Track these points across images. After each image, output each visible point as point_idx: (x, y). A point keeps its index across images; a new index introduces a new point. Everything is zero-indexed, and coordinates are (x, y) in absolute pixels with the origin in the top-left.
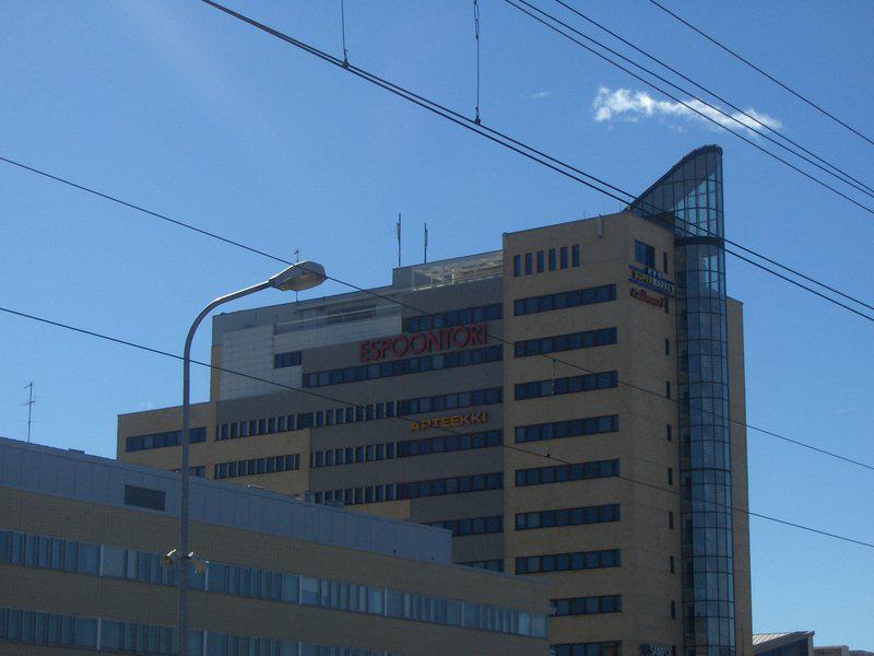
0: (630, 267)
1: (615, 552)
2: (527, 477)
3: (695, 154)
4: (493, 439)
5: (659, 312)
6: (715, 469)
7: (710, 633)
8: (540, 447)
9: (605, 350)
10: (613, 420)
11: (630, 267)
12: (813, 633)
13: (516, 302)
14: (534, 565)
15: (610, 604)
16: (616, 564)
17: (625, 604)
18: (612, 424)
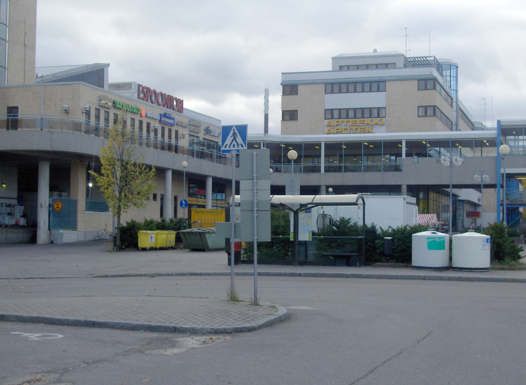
12: (108, 65)
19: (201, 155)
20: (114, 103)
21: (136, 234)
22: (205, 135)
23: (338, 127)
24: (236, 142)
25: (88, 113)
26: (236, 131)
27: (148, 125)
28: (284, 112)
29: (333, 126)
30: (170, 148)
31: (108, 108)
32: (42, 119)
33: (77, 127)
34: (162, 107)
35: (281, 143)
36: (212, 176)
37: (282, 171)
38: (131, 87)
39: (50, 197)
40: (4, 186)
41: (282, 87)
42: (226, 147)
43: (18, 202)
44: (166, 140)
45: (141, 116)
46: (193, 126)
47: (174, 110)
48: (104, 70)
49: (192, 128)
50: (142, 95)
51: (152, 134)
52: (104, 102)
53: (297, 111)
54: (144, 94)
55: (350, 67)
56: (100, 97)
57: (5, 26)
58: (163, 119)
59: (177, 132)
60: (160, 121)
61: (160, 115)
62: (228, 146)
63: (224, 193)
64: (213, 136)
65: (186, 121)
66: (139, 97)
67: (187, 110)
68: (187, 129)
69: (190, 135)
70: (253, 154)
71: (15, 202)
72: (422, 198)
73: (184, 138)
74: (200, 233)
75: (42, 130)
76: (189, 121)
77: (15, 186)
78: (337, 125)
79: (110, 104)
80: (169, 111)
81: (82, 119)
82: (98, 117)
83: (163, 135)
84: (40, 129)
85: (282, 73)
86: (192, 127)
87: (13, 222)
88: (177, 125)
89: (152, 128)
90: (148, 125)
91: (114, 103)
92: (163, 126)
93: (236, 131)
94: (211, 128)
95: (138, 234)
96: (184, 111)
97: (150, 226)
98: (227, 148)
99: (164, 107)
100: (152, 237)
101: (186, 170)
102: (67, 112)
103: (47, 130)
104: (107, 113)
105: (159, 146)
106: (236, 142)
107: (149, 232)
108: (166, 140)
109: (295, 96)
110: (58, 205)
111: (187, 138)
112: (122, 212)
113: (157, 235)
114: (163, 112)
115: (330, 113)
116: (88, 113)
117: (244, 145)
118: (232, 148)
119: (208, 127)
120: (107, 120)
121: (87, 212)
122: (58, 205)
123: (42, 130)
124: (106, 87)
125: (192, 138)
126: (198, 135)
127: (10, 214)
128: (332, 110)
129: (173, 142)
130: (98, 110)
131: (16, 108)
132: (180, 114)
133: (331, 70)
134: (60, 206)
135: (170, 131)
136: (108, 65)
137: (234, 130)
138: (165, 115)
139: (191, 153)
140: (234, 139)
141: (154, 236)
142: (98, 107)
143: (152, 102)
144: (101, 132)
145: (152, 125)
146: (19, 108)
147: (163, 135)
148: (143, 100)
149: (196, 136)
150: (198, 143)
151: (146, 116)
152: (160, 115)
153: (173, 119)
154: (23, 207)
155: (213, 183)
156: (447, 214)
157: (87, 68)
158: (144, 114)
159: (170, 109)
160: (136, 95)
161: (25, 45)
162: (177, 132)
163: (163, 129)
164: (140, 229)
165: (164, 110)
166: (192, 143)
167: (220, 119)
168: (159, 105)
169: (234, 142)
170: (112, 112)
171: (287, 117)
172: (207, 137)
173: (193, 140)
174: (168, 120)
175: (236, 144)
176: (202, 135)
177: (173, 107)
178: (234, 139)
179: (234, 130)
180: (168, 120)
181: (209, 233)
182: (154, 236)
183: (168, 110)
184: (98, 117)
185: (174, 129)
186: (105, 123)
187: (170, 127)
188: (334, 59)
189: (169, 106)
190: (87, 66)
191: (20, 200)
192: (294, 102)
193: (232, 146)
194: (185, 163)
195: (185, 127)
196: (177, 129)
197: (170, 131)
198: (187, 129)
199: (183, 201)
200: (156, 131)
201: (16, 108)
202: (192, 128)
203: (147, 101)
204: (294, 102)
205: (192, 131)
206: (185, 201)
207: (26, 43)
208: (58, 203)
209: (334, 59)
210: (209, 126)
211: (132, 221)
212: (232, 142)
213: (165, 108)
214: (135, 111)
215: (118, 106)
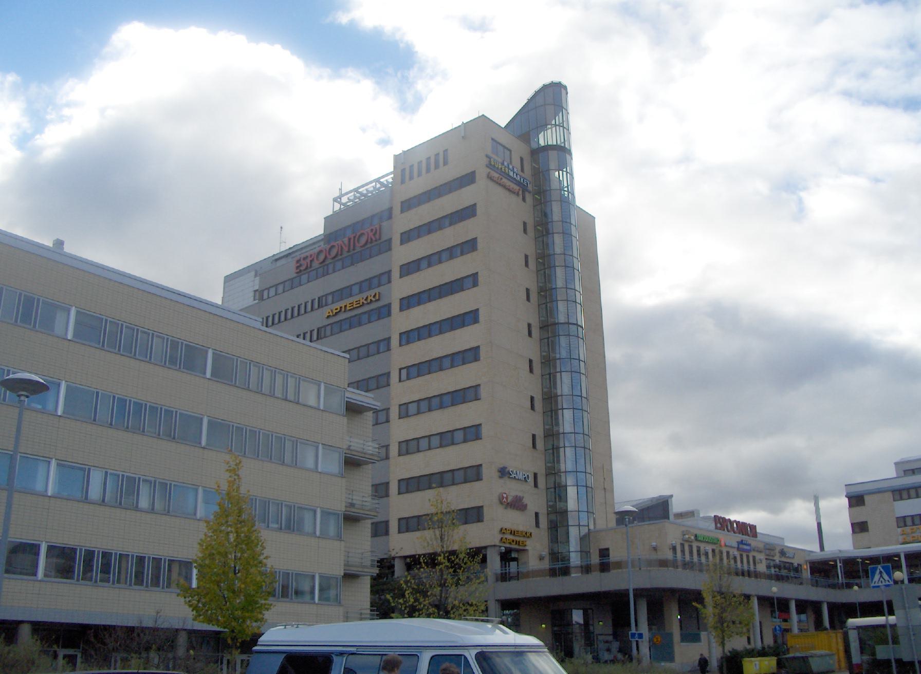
0: (487, 156)
1: (479, 509)
2: (408, 337)
3: (545, 87)
4: (384, 312)
5: (515, 201)
6: (575, 433)
7: (571, 545)
8: (418, 458)
9: (469, 223)
10: (475, 276)
11: (487, 156)
12: (671, 496)
13: (399, 481)
14: (413, 408)
15: (473, 433)
16: (478, 437)
17: (484, 431)
18: (473, 279)
19: (779, 578)
20: (696, 536)
21: (741, 662)
22: (780, 557)
23: (914, 535)
24: (883, 579)
25: (674, 549)
26: (882, 570)
27: (728, 553)
28: (852, 525)
29: (908, 534)
30: (749, 574)
31: (691, 542)
32: (639, 559)
33: (663, 563)
34: (737, 535)
35: (858, 557)
36: (756, 595)
37: (863, 586)
38: (694, 515)
39: (649, 631)
40: (544, 626)
41: (847, 499)
42: (875, 583)
43: (614, 638)
44: (687, 557)
45: (721, 546)
46: (768, 549)
47: (748, 536)
48: (668, 502)
49: (767, 552)
50: (719, 525)
51: (732, 562)
52: (687, 536)
53: (866, 522)
54: (721, 524)
55: (916, 471)
56: (683, 532)
57: (590, 475)
58: (741, 546)
59: (754, 557)
60: (738, 549)
61: (738, 542)
62: (876, 583)
63: (804, 613)
64: (788, 557)
65: (761, 546)
66: (716, 528)
67: (760, 533)
68: (763, 554)
69: (766, 559)
70: (902, 588)
71: (610, 638)
72: (559, 411)
73: (761, 563)
74: (802, 657)
75: (640, 569)
76: (765, 546)
77: (610, 622)
78: (912, 533)
79: (693, 538)
80: (745, 537)
81: (669, 555)
82: (683, 551)
83: (742, 562)
84: (638, 569)
85: (846, 485)
86: (767, 551)
87: (611, 657)
88: (754, 550)
89: (731, 557)
90: (728, 553)
91: (696, 536)
92: (741, 553)
93: (882, 570)
94: (785, 550)
95: (743, 662)
96: (758, 535)
97: (751, 653)
98: (876, 584)
99: (739, 533)
100: (756, 664)
101: (775, 596)
102: (655, 549)
103: (645, 569)
104: (691, 547)
105: (680, 563)
106: (883, 579)
107: (753, 659)
108: (687, 557)
109: (862, 507)
110: (657, 638)
111: (764, 562)
112: (725, 642)
113: (760, 661)
114: (739, 540)
115: (902, 521)
116: (674, 549)
117: (890, 581)
118: (880, 584)
119: (783, 549)
120: (691, 553)
121: (682, 644)
122: (657, 638)
123: (640, 569)
124: (671, 517)
125: (768, 562)
126: (775, 558)
127: (608, 650)
128: (904, 517)
129: (746, 568)
130: (682, 545)
131: (608, 549)
132: (755, 539)
133: (895, 476)
134: (659, 640)
135: (748, 556)
136: (671, 496)
137: (880, 569)
138: (742, 542)
139: (770, 577)
140: (881, 576)
141: (757, 663)
142: (683, 542)
143: (728, 531)
144: (746, 574)
145: (731, 553)
146: (610, 549)
147: (742, 562)
148: (720, 529)
149: (771, 560)
150: (775, 566)
151: (726, 546)
152: (738, 542)
153: (749, 545)
154: (618, 643)
155: (797, 606)
156: (367, 609)
157: (652, 501)
158: (723, 543)
159: (746, 535)
160: (713, 525)
161: (605, 489)
162: (754, 557)
163: (741, 556)
164: (742, 657)
165: (740, 537)
166: (768, 567)
167: (783, 537)
168: (734, 532)
169: (881, 579)
170: (695, 545)
171: (857, 530)
172: (784, 559)
173: (770, 563)
174: (745, 547)
175: (883, 580)
176: (777, 559)
177: (748, 533)
178: (881, 576)
179: (880, 569)
180: (745, 547)
181: (811, 656)
182: (757, 663)
183: (744, 536)
184: (683, 551)
185: (751, 554)
186: (690, 556)
187: (748, 554)
188: (896, 464)
189: (744, 533)
190: (652, 499)
191: (615, 635)
192: (862, 514)
193: (880, 582)
194: (774, 589)
195: (761, 552)
196: (754, 555)
197: (748, 556)
198: (763, 554)
199: (777, 627)
200: (735, 558)
201: (608, 549)
202: (767, 552)
203: (724, 530)
204: (862, 514)
205: (768, 555)
206: (779, 626)
207: (605, 487)
208: (657, 637)
209: (896, 464)
210: (783, 548)
211: (733, 649)
212: (880, 579)
213: (740, 535)
214: (715, 542)
215: (700, 539)
